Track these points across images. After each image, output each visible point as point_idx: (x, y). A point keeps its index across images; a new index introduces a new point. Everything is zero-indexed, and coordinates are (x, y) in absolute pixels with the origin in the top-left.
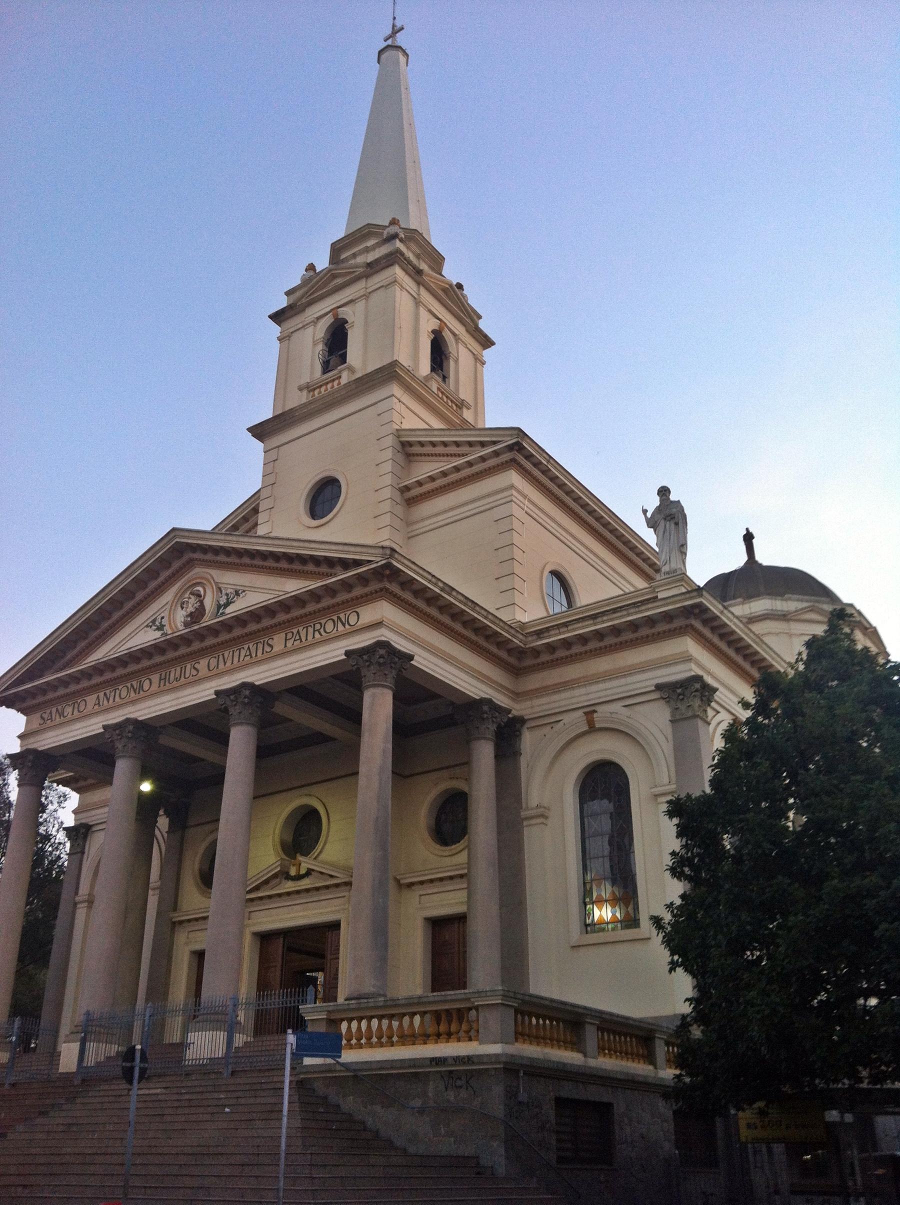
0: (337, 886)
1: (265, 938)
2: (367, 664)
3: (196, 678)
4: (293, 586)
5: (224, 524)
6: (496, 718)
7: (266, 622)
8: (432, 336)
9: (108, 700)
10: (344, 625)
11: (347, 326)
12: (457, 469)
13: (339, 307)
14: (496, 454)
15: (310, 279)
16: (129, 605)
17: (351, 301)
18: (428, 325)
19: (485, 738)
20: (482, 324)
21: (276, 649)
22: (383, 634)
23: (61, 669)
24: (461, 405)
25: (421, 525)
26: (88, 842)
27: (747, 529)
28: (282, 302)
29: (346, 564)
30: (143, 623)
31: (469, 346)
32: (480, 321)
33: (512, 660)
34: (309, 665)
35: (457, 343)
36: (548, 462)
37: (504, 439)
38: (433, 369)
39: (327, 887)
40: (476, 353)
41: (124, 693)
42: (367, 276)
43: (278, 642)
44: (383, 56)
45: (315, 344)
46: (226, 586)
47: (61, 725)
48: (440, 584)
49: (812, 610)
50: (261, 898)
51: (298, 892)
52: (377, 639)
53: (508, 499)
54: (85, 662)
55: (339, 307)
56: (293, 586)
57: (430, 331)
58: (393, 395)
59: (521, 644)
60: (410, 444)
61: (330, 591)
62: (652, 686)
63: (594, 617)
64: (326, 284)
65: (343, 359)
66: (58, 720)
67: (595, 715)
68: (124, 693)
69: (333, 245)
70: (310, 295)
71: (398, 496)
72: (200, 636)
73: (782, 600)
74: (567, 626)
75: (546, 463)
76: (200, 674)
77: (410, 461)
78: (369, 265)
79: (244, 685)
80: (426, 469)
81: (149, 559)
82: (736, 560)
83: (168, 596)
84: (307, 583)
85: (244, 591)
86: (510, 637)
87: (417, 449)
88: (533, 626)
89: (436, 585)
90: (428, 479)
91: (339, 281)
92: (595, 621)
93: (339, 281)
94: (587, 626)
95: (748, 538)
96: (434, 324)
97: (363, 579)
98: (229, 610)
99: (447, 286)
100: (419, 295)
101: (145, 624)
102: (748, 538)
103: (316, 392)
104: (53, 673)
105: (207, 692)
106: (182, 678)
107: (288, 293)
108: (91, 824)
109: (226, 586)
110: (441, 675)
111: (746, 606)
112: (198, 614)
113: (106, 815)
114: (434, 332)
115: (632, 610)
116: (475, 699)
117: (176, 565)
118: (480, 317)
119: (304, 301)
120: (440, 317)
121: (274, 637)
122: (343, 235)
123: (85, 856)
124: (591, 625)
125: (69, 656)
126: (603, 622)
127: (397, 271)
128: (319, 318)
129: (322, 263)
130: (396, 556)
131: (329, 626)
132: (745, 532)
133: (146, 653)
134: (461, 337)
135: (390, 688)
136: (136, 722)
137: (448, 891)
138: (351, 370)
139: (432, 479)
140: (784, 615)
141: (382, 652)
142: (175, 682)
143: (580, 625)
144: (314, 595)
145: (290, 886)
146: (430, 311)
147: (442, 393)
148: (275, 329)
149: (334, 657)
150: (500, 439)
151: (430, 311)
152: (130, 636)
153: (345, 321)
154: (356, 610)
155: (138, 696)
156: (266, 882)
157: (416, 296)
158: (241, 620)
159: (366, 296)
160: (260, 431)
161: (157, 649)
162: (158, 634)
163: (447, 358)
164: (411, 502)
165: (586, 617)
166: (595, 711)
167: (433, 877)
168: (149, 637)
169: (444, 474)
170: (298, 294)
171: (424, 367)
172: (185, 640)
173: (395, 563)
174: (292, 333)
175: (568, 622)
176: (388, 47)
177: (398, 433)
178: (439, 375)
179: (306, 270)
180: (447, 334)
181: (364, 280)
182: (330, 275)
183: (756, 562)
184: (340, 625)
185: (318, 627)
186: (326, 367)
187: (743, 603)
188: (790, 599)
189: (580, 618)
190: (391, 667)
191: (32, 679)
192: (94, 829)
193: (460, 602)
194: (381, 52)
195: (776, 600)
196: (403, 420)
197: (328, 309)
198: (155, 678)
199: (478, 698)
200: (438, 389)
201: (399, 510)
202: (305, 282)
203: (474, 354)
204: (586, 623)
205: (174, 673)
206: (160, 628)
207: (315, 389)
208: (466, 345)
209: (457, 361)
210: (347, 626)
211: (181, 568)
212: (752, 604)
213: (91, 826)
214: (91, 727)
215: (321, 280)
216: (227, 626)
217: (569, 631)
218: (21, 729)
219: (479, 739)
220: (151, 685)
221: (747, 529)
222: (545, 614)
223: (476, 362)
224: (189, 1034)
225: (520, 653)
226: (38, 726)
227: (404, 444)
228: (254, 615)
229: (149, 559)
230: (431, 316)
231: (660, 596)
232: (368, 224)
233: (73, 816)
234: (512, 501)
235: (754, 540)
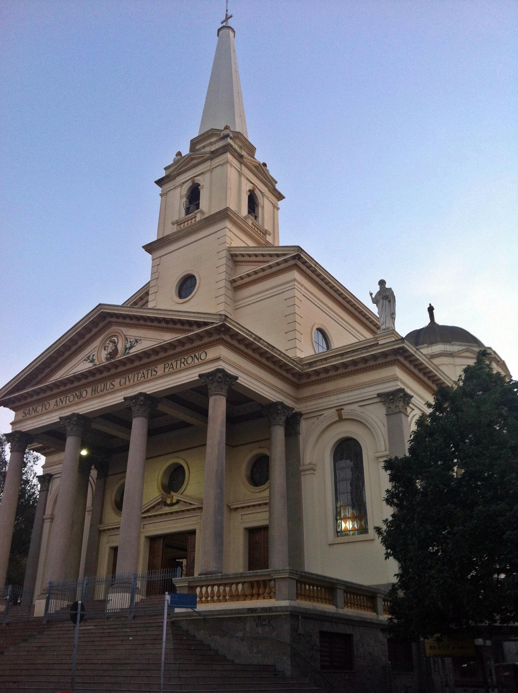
0: (194, 509)
1: (152, 540)
2: (211, 382)
3: (113, 390)
4: (168, 337)
5: (129, 301)
6: (285, 413)
7: (153, 358)
8: (249, 193)
9: (62, 403)
10: (198, 359)
11: (200, 187)
12: (263, 270)
13: (195, 177)
14: (286, 261)
15: (179, 160)
16: (74, 348)
17: (202, 173)
18: (246, 187)
19: (279, 425)
20: (278, 187)
21: (159, 373)
22: (221, 365)
23: (35, 385)
24: (265, 233)
25: (242, 302)
26: (51, 484)
27: (430, 304)
28: (162, 174)
29: (199, 324)
30: (82, 359)
31: (270, 199)
32: (276, 184)
33: (295, 380)
34: (167, 386)
35: (263, 197)
36: (316, 265)
37: (290, 252)
38: (249, 212)
39: (188, 510)
40: (274, 203)
41: (71, 399)
42: (211, 159)
43: (160, 369)
44: (221, 32)
45: (181, 198)
46: (130, 337)
47: (35, 417)
48: (254, 336)
49: (467, 351)
50: (150, 517)
51: (171, 513)
52: (217, 367)
53: (293, 287)
54: (49, 381)
55: (195, 177)
56: (168, 337)
57: (247, 190)
58: (226, 227)
59: (300, 371)
60: (236, 255)
61: (190, 340)
62: (375, 394)
63: (342, 355)
64: (187, 164)
65: (198, 206)
66: (33, 414)
67: (343, 411)
68: (71, 399)
69: (192, 141)
70: (179, 170)
71: (229, 285)
72: (115, 365)
73: (450, 345)
74: (326, 360)
75: (314, 266)
76: (115, 388)
77: (236, 265)
78: (212, 152)
79: (141, 394)
80: (245, 270)
81: (86, 321)
82: (424, 322)
83: (97, 343)
84: (177, 335)
85: (140, 340)
86: (294, 367)
87: (240, 258)
88: (307, 360)
89: (251, 336)
90: (246, 276)
91: (195, 161)
92: (343, 357)
93: (195, 161)
94: (338, 360)
95: (431, 309)
96: (250, 186)
97: (209, 333)
98: (132, 351)
99: (257, 165)
100: (241, 169)
101: (84, 359)
102: (431, 309)
103: (182, 225)
104: (30, 387)
105: (119, 398)
106: (105, 390)
107: (166, 169)
108: (52, 474)
109: (130, 337)
110: (254, 388)
111: (430, 349)
112: (114, 353)
113: (61, 469)
114: (250, 191)
115: (364, 351)
116: (274, 402)
117: (101, 325)
118: (276, 182)
119: (175, 173)
120: (254, 182)
121: (158, 366)
122: (197, 135)
123: (49, 493)
124: (340, 359)
125: (40, 377)
126: (347, 358)
127: (229, 156)
128: (183, 183)
129: (186, 151)
130: (228, 320)
131: (190, 360)
132: (429, 306)
133: (84, 375)
134: (265, 194)
135: (225, 396)
136: (78, 415)
137: (258, 512)
138: (202, 213)
139: (249, 275)
140: (451, 354)
141: (220, 375)
142: (101, 392)
143: (334, 359)
144: (181, 342)
145: (167, 509)
146: (248, 179)
147: (255, 226)
148: (159, 190)
149: (192, 378)
150: (288, 253)
151: (248, 179)
152: (75, 366)
153: (199, 185)
154: (205, 351)
155: (79, 400)
156: (153, 507)
157: (239, 170)
158: (139, 357)
159: (211, 170)
160: (150, 248)
161: (91, 373)
162: (91, 365)
163: (258, 206)
164: (236, 289)
165: (337, 355)
166: (342, 409)
167: (249, 504)
168: (86, 366)
169: (256, 273)
170: (172, 169)
171: (244, 211)
172: (107, 368)
173: (227, 324)
174: (168, 191)
175: (327, 358)
176: (223, 27)
177: (229, 249)
178: (252, 216)
179: (176, 155)
180: (257, 192)
181: (209, 161)
182: (190, 158)
183: (435, 323)
184: (196, 359)
185: (183, 360)
186: (188, 211)
187: (428, 347)
188: (455, 344)
189: (334, 356)
190: (225, 384)
191: (18, 391)
192: (54, 477)
193: (265, 346)
194: (219, 30)
195: (446, 345)
196: (232, 242)
197: (189, 178)
198: (89, 390)
199: (275, 401)
200: (252, 224)
201: (230, 293)
202: (176, 162)
203: (273, 204)
204: (337, 359)
205: (100, 387)
206: (92, 361)
207: (181, 224)
208: (268, 198)
209: (263, 208)
210: (200, 360)
211: (104, 327)
212: (433, 348)
213: (52, 475)
214: (53, 418)
215: (185, 161)
216: (130, 360)
217: (327, 363)
218: (12, 419)
219: (275, 425)
220: (87, 394)
221: (430, 304)
222: (314, 353)
223: (274, 208)
224: (109, 595)
225: (299, 375)
226: (22, 417)
227: (232, 256)
228: (146, 354)
229: (86, 321)
230: (248, 182)
231: (380, 343)
232: (212, 129)
233: (42, 469)
234: (294, 288)
235: (434, 311)
